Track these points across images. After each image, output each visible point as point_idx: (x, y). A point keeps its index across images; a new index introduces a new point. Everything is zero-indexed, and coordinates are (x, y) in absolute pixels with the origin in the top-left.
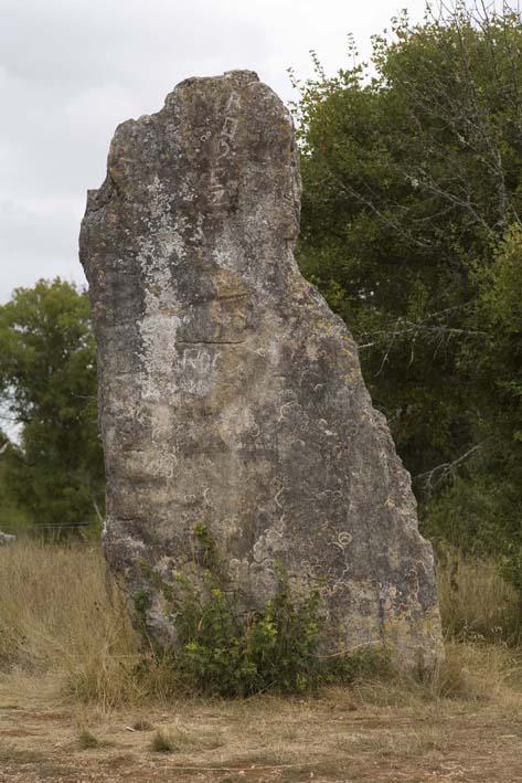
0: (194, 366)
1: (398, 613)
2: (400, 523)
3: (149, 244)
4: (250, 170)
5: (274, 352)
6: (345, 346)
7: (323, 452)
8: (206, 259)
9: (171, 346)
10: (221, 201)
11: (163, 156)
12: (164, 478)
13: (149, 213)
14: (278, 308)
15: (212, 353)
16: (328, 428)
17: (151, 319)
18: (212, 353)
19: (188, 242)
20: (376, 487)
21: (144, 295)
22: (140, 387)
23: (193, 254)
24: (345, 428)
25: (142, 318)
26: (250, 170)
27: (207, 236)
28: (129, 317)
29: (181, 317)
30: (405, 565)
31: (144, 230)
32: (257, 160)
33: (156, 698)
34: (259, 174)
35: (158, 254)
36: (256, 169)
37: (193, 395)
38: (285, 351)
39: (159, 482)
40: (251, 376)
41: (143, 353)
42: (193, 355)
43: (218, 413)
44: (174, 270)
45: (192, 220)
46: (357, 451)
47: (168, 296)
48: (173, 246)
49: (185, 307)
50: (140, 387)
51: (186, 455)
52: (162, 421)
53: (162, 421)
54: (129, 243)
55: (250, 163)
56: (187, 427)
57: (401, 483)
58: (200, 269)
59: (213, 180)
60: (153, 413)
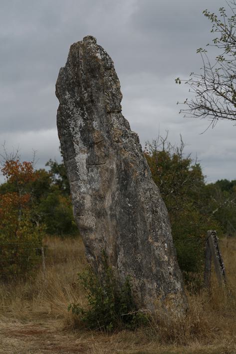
0: (93, 176)
1: (158, 297)
2: (154, 250)
3: (73, 122)
4: (93, 82)
5: (114, 166)
6: (131, 162)
7: (129, 214)
8: (91, 126)
9: (85, 167)
10: (88, 99)
11: (67, 82)
12: (91, 228)
13: (69, 108)
14: (85, 140)
15: (98, 169)
16: (129, 202)
17: (78, 156)
18: (98, 169)
19: (84, 119)
20: (145, 232)
21: (73, 145)
22: (80, 187)
23: (86, 124)
24: (134, 202)
25: (75, 156)
26: (93, 82)
27: (89, 116)
28: (72, 156)
29: (87, 154)
30: (158, 272)
31: (69, 116)
32: (94, 77)
33: (212, 299)
34: (97, 83)
35: (76, 126)
36: (95, 81)
37: (95, 189)
38: (117, 166)
39: (91, 229)
40: (110, 179)
41: (77, 171)
42: (92, 171)
43: (105, 197)
44: (81, 132)
45: (82, 109)
46: (138, 214)
47: (81, 145)
48: (80, 122)
49: (88, 149)
50: (80, 187)
51: (98, 217)
52: (88, 202)
53: (88, 202)
54: (66, 123)
55: (93, 79)
56: (96, 204)
57: (157, 230)
58: (89, 131)
59: (83, 90)
60: (85, 198)
